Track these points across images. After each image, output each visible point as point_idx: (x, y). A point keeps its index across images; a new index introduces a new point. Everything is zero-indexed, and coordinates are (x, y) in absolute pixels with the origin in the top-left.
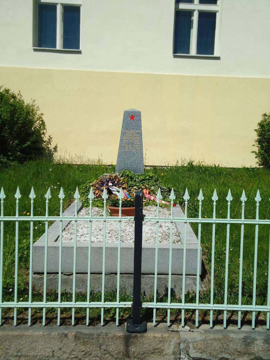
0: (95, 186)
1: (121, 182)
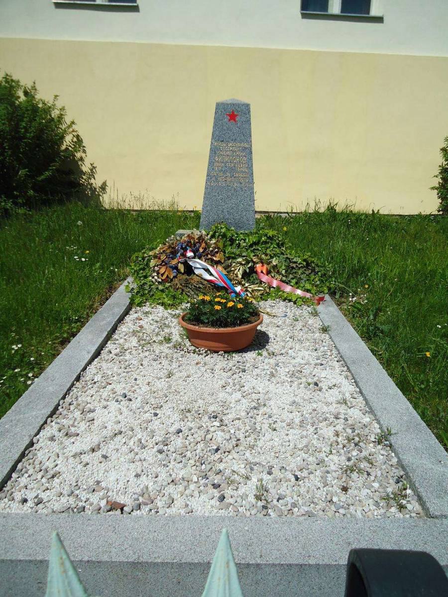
0: (160, 258)
1: (211, 249)
